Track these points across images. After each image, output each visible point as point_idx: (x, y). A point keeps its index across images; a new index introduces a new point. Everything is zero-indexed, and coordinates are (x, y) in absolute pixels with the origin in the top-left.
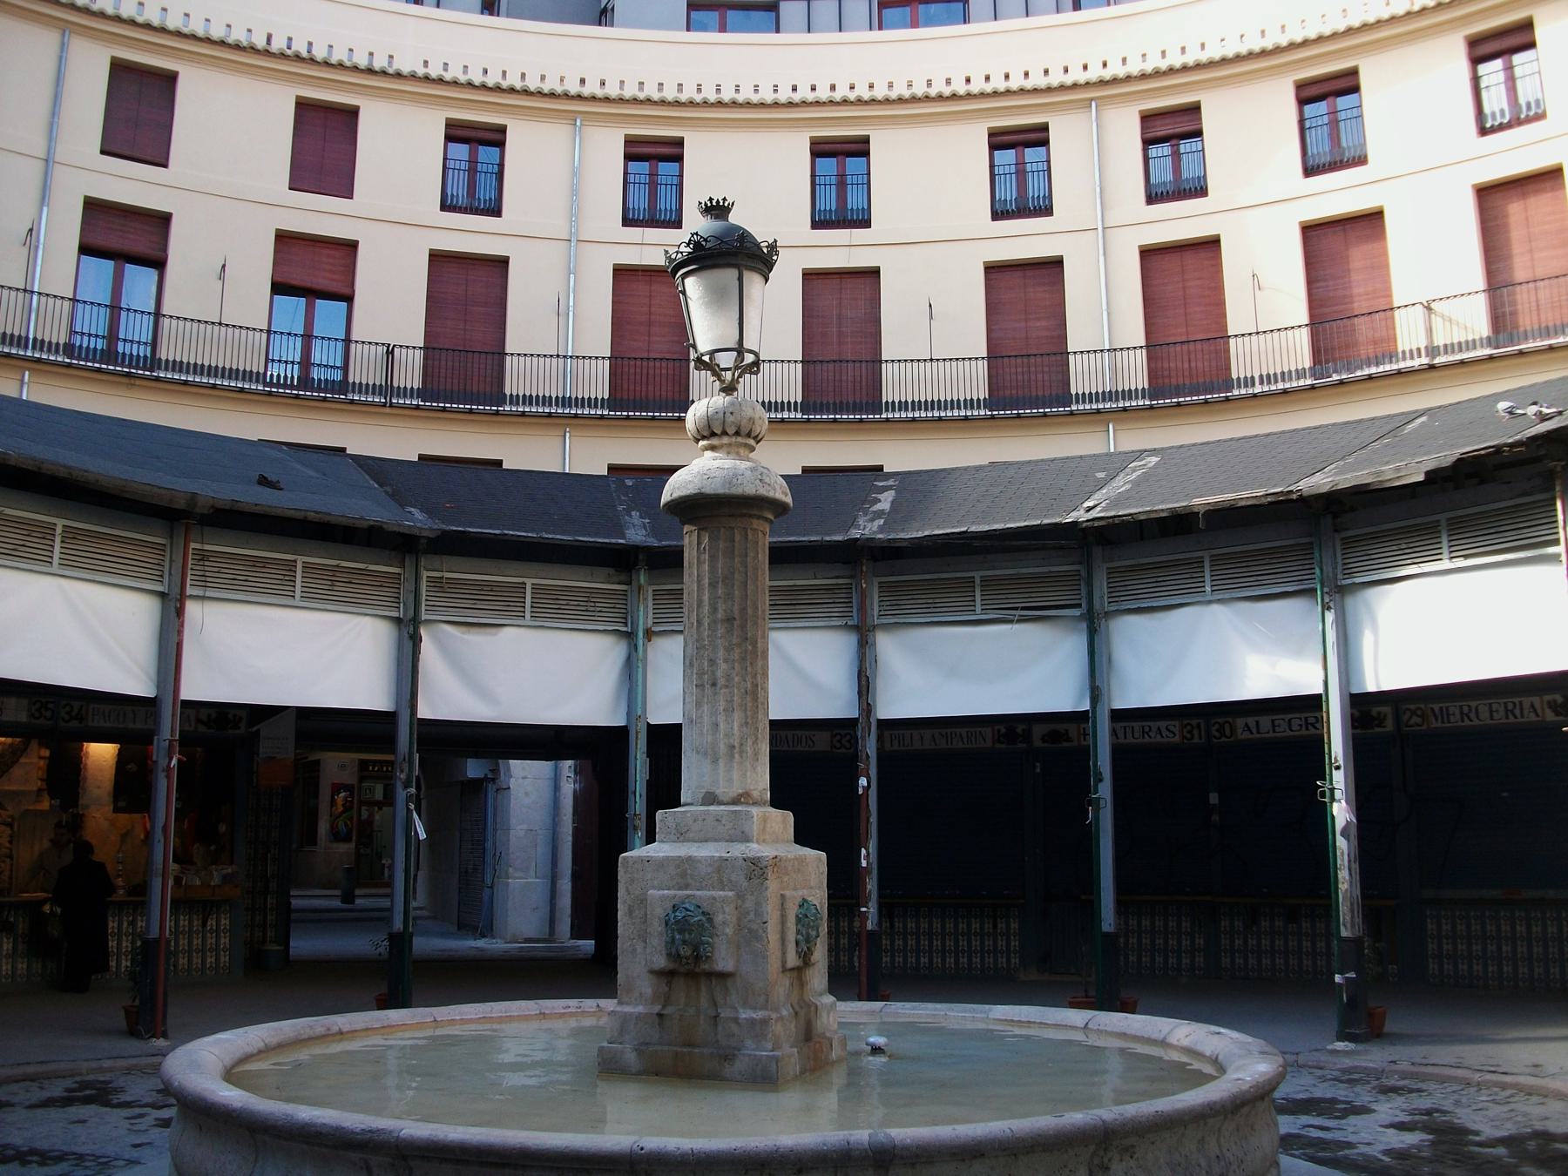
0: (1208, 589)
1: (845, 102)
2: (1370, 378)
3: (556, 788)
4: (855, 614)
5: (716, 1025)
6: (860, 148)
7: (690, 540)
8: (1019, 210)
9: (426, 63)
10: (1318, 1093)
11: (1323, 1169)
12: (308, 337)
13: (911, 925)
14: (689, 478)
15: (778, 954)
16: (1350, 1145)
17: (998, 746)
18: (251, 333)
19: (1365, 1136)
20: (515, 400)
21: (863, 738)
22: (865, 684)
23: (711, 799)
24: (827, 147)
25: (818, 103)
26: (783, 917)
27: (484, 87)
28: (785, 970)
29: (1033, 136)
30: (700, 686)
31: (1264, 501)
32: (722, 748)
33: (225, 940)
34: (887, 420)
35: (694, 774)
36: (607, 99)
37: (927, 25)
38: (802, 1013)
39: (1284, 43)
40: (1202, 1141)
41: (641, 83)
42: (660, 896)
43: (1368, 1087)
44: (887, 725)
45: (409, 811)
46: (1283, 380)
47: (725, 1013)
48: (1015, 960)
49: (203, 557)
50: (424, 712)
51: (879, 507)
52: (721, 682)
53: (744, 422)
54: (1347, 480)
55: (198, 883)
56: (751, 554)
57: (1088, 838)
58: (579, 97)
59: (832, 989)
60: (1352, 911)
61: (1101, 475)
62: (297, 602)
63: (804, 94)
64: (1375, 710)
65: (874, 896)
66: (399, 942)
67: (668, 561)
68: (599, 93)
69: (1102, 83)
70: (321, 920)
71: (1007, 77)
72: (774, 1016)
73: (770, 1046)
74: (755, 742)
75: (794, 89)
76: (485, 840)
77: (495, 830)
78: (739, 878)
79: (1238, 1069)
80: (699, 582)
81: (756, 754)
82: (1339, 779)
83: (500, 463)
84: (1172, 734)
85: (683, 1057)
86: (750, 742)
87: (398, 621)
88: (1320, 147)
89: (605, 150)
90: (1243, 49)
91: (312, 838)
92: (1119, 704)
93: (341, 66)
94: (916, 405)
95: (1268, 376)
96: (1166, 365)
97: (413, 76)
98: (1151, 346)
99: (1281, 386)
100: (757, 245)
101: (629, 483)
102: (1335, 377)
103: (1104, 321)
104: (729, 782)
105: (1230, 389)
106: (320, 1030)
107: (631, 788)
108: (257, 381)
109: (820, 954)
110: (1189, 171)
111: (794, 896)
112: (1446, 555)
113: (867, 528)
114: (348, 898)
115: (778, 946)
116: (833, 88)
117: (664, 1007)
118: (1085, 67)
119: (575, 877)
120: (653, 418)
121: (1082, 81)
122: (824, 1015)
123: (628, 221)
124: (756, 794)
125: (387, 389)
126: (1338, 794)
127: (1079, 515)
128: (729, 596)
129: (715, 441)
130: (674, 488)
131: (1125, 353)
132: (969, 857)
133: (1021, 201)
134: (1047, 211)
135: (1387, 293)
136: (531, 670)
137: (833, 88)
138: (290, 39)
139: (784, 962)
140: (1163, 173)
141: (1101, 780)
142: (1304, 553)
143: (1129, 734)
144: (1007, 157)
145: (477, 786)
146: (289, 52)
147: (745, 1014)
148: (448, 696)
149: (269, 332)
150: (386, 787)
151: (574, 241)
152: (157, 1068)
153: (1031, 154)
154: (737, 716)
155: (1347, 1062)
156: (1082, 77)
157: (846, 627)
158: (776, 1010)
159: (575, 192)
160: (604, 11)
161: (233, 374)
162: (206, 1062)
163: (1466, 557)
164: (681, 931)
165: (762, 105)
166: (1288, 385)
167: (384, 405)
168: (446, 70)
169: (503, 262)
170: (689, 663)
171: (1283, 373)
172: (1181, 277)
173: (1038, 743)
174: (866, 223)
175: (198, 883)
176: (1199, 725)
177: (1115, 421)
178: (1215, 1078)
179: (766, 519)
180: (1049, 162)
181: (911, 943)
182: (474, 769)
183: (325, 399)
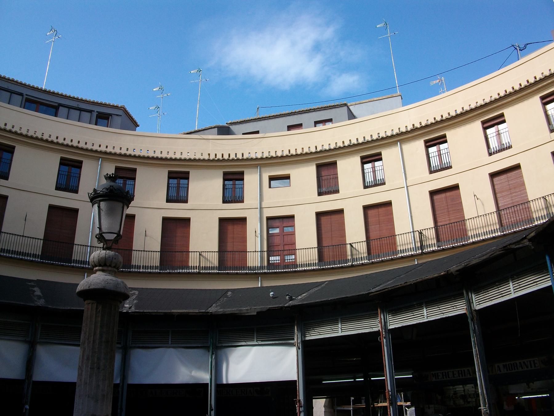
0: (170, 342)
29: (76, 164)
46: (150, 269)
67: (78, 315)
88: (173, 193)
98: (162, 251)
102: (168, 271)
112: (255, 340)
129: (105, 268)
135: (188, 246)
149: (413, 232)
157: (25, 342)
163: (262, 341)
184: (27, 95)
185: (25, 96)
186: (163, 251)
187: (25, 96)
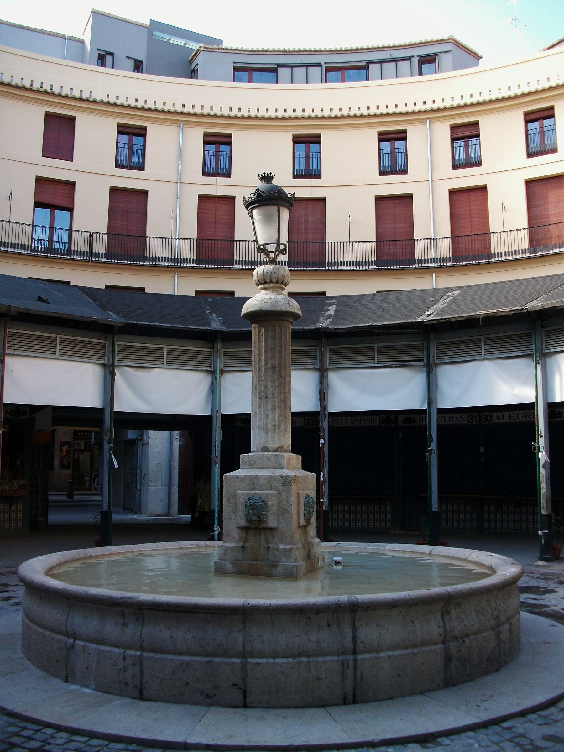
1: (310, 118)
2: (556, 254)
3: (171, 443)
4: (318, 363)
5: (268, 551)
6: (316, 140)
7: (255, 330)
8: (392, 171)
9: (108, 95)
10: (531, 584)
11: (537, 616)
12: (52, 228)
13: (341, 508)
14: (255, 302)
15: (296, 519)
16: (546, 606)
17: (382, 425)
18: (24, 226)
19: (553, 602)
20: (151, 259)
21: (322, 421)
22: (323, 396)
23: (265, 449)
24: (301, 139)
25: (297, 118)
26: (298, 503)
27: (136, 108)
28: (299, 527)
30: (260, 398)
31: (510, 313)
32: (270, 426)
33: (20, 515)
34: (328, 270)
35: (257, 438)
36: (195, 115)
37: (348, 81)
38: (306, 546)
39: (519, 93)
40: (489, 601)
41: (212, 107)
42: (242, 493)
43: (553, 581)
44: (333, 415)
45: (110, 455)
46: (516, 254)
47: (272, 546)
48: (389, 524)
49: (13, 335)
50: (116, 408)
51: (329, 313)
52: (270, 396)
53: (280, 277)
54: (548, 304)
55: (7, 488)
56: (283, 338)
57: (426, 467)
58: (182, 113)
59: (318, 536)
60: (547, 502)
61: (433, 299)
62: (57, 357)
63: (290, 113)
64: (557, 410)
65: (327, 494)
66: (106, 516)
67: (246, 337)
68: (192, 111)
69: (432, 111)
70: (60, 506)
71: (387, 107)
72: (295, 547)
73: (293, 560)
74: (285, 424)
75: (285, 111)
76: (137, 468)
77: (142, 464)
78: (279, 485)
79: (504, 570)
80: (259, 350)
81: (285, 429)
82: (542, 442)
83: (143, 289)
84: (463, 420)
85: (252, 566)
86: (283, 424)
87: (104, 366)
88: (535, 144)
89: (195, 138)
90: (500, 96)
91: (51, 467)
92: (441, 406)
93: (67, 97)
94: (342, 264)
95: (509, 252)
96: (460, 246)
97: (102, 102)
99: (514, 257)
100: (286, 195)
101: (210, 300)
102: (540, 253)
103: (432, 225)
104: (273, 442)
105: (490, 257)
106: (82, 555)
107: (213, 444)
108: (28, 249)
109: (313, 520)
110: (473, 154)
111: (304, 493)
113: (324, 323)
114: (70, 496)
115: (296, 515)
116: (304, 110)
117: (244, 543)
118: (425, 103)
119: (180, 485)
120: (217, 268)
121: (423, 110)
122: (315, 547)
123: (205, 174)
124: (285, 447)
125: (90, 253)
126: (541, 449)
127: (423, 318)
128: (273, 357)
129: (266, 286)
130: (247, 308)
131: (441, 240)
132: (380, 475)
133: (393, 167)
134: (405, 172)
136: (168, 389)
137: (304, 110)
138: (42, 83)
139: (299, 523)
140: (460, 155)
141: (432, 441)
142: (527, 338)
143: (443, 420)
144: (386, 145)
145: (133, 443)
146: (42, 90)
147: (282, 546)
148: (128, 401)
149: (33, 226)
150: (85, 443)
151: (179, 182)
152: (15, 573)
153: (398, 144)
154: (277, 411)
155: (544, 570)
156: (423, 108)
157: (314, 369)
158: (295, 544)
159: (180, 159)
160: (193, 71)
161: (16, 246)
162: (37, 568)
164: (252, 509)
165: (270, 118)
166: (518, 257)
167: (89, 261)
168: (117, 99)
169: (145, 193)
170: (255, 387)
171: (515, 251)
172: (468, 203)
173: (400, 424)
174: (319, 176)
175: (7, 488)
176: (475, 416)
177: (436, 272)
178: (492, 575)
179: (290, 322)
180: (406, 148)
181: (341, 516)
182: (131, 434)
183: (60, 258)
184: (326, 63)
185: (324, 66)
186: (532, 227)
187: (324, 66)
